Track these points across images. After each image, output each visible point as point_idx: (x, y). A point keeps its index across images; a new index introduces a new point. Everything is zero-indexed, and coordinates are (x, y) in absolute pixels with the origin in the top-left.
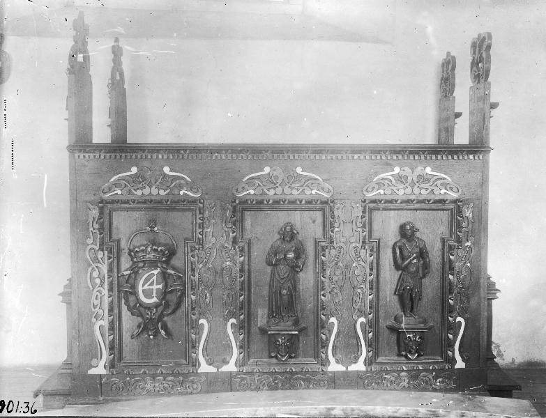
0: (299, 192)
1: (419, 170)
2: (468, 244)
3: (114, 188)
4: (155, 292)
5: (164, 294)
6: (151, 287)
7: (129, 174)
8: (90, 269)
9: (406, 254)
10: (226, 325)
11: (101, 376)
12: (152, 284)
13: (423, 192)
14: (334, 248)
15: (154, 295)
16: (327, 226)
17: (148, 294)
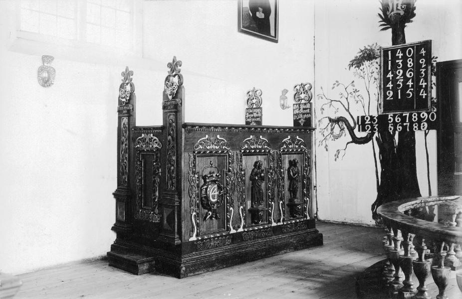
12: (215, 192)
15: (216, 197)
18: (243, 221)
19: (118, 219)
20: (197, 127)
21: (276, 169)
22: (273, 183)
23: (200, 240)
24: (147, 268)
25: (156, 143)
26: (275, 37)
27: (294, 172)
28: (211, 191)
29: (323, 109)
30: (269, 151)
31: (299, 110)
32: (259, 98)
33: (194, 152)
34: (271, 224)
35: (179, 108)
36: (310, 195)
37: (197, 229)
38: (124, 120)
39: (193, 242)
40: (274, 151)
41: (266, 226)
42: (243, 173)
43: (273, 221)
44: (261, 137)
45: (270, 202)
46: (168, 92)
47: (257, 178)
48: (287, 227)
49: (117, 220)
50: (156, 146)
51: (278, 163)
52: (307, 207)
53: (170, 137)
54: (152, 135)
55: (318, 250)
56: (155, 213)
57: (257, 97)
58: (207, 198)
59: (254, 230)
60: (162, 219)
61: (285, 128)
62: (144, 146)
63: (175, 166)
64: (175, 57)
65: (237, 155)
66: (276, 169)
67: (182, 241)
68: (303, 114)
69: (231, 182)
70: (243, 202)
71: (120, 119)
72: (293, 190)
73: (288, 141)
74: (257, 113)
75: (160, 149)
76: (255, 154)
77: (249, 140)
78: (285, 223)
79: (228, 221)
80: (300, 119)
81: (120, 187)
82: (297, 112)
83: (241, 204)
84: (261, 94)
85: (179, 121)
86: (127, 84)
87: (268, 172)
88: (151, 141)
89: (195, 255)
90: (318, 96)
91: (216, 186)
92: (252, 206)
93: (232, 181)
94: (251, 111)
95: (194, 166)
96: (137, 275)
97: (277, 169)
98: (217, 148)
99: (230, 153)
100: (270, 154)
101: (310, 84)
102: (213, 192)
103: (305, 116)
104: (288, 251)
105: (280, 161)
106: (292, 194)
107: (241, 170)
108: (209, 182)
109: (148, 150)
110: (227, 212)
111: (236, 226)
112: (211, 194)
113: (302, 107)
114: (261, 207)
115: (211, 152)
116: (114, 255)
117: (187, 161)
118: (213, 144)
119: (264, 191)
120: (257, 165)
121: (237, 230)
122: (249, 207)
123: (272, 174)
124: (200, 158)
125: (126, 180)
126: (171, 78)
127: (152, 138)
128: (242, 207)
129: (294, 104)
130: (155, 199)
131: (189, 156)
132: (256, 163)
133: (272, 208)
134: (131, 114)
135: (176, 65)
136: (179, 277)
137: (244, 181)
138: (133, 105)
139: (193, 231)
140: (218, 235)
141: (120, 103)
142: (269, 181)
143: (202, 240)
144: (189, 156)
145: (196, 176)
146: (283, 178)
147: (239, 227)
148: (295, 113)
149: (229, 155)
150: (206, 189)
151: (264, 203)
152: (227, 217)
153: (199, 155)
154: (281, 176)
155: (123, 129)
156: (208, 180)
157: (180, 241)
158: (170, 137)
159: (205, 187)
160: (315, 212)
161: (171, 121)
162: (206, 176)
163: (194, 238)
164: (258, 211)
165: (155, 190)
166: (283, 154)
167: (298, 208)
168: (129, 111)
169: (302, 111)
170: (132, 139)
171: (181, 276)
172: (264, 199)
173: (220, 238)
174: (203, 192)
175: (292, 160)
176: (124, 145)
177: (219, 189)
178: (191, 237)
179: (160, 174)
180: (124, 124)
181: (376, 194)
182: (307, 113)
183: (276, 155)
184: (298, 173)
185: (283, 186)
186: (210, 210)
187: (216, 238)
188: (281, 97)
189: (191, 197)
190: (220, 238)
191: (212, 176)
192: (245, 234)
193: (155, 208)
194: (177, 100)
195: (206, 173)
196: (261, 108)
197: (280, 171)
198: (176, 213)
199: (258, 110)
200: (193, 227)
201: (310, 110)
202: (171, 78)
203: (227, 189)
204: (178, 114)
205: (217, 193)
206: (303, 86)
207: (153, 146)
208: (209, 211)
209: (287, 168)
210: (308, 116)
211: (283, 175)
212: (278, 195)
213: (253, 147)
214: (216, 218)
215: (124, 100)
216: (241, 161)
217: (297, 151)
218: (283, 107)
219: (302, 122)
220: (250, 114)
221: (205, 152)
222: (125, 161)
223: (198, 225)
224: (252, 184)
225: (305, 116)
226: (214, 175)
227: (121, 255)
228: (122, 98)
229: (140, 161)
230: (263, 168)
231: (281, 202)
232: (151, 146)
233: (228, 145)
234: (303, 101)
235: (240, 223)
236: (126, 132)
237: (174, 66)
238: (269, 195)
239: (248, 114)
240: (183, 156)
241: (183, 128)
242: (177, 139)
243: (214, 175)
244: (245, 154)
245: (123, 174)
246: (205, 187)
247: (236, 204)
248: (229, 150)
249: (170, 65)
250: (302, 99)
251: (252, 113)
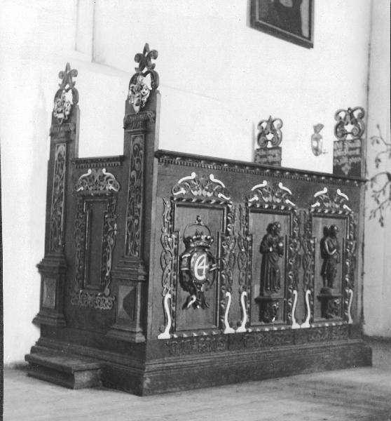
6: (202, 267)
12: (203, 265)
18: (246, 316)
19: (43, 306)
20: (178, 158)
21: (302, 239)
22: (296, 259)
23: (176, 339)
24: (89, 379)
25: (111, 182)
26: (310, 38)
27: (332, 246)
28: (197, 262)
29: (379, 160)
30: (293, 209)
31: (343, 150)
32: (278, 132)
33: (172, 198)
34: (292, 324)
35: (150, 126)
36: (354, 285)
37: (172, 322)
38: (60, 148)
39: (163, 341)
40: (300, 209)
41: (283, 328)
42: (249, 239)
43: (294, 320)
44: (281, 185)
45: (291, 291)
46: (135, 101)
47: (271, 250)
48: (317, 333)
49: (42, 307)
50: (111, 187)
51: (305, 230)
52: (350, 303)
53: (134, 173)
54: (104, 170)
55: (363, 370)
56: (104, 295)
57: (274, 132)
58: (190, 273)
59: (263, 332)
60: (115, 305)
61: (319, 175)
62: (91, 189)
63: (140, 218)
64: (147, 45)
65: (240, 209)
66: (302, 239)
67: (146, 338)
68: (349, 157)
69: (229, 252)
70: (248, 285)
71: (53, 146)
72: (328, 274)
73: (324, 196)
74: (274, 156)
75: (117, 194)
76: (269, 211)
77: (261, 189)
78: (313, 326)
79: (222, 313)
80: (343, 165)
81: (49, 254)
82: (339, 153)
83: (245, 289)
84: (282, 126)
85: (150, 147)
86: (67, 91)
87: (290, 242)
88: (102, 181)
89: (170, 361)
90: (372, 138)
91: (205, 255)
92: (261, 294)
93: (231, 251)
94: (263, 153)
95: (172, 220)
96: (72, 388)
97: (304, 238)
98: (209, 195)
99: (230, 206)
100: (295, 214)
101: (362, 109)
102: (200, 265)
103: (352, 160)
104: (317, 370)
105: (309, 225)
107: (247, 234)
108: (194, 248)
109: (96, 195)
110: (221, 299)
111: (235, 322)
112: (196, 268)
113: (347, 145)
114: (274, 296)
115: (199, 201)
116: (34, 359)
117: (160, 211)
118: (203, 188)
119: (282, 272)
120: (272, 229)
121: (235, 329)
122: (256, 294)
123: (295, 246)
124: (181, 209)
125: (60, 244)
126: (140, 78)
127: (104, 176)
128: (245, 293)
129: (335, 142)
130: (105, 272)
131: (164, 203)
132: (270, 226)
133: (293, 300)
134: (72, 138)
135: (149, 57)
136: (139, 393)
137: (251, 251)
138: (75, 125)
139: (165, 323)
140: (205, 334)
141: (55, 120)
142: (291, 256)
143: (181, 338)
144: (164, 203)
145: (174, 236)
146: (314, 253)
147: (239, 325)
148: (336, 155)
149: (228, 208)
150: (190, 258)
151: (281, 291)
152: (221, 307)
153: (180, 203)
154: (310, 250)
155: (58, 163)
156: (192, 245)
157: (143, 339)
158: (134, 173)
159: (187, 255)
160: (362, 241)
161: (136, 146)
162: (190, 238)
163: (165, 335)
164: (271, 301)
165: (105, 257)
166: (315, 216)
167: (335, 303)
168: (68, 133)
169: (346, 152)
170: (70, 180)
171: (145, 393)
172: (282, 283)
173: (208, 339)
174: (184, 263)
175: (329, 227)
176: (58, 188)
177: (209, 261)
178: (161, 331)
179: (115, 232)
180: (59, 155)
182: (356, 156)
183: (302, 217)
184: (338, 248)
185: (314, 266)
186: (194, 292)
187: (202, 339)
188: (313, 136)
189: (163, 270)
190: (208, 339)
191: (199, 239)
192: (248, 337)
193: (104, 287)
194: (148, 113)
195: (190, 233)
196: (280, 149)
197: (309, 242)
198: (139, 296)
199: (275, 152)
200: (166, 318)
201: (361, 151)
202: (140, 78)
203: (222, 262)
204: (149, 135)
205: (206, 267)
206: (350, 112)
207: (105, 189)
208: (192, 294)
209: (320, 240)
210: (355, 160)
211: (313, 249)
212: (304, 280)
213: (266, 200)
214: (203, 306)
215: (61, 116)
216: (247, 221)
217: (337, 212)
218: (317, 151)
219: (346, 170)
220: (261, 157)
221: (189, 200)
222: (59, 213)
223: (174, 315)
224: (264, 258)
225: (352, 160)
226: (203, 237)
228: (58, 112)
229: (83, 213)
230: (281, 234)
231: (308, 292)
232: (102, 188)
233: (226, 192)
234: (349, 137)
235: (242, 319)
236: (62, 168)
237: (145, 59)
238: (289, 279)
239: (258, 157)
240: (153, 202)
241: (156, 157)
242: (145, 175)
243: (203, 237)
244: (254, 209)
245: (55, 235)
246: (187, 255)
247: (235, 286)
248: (229, 201)
249: (139, 58)
250: (347, 133)
251: (265, 156)
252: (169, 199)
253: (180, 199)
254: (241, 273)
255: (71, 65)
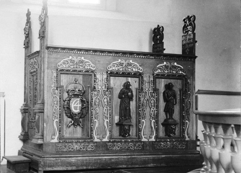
0: (82, 68)
1: (172, 64)
2: (189, 93)
3: (158, 69)
4: (78, 107)
5: (82, 109)
6: (77, 105)
7: (163, 64)
8: (103, 98)
9: (169, 95)
10: (53, 122)
11: (153, 142)
12: (77, 104)
13: (174, 72)
14: (144, 92)
15: (78, 108)
16: (141, 82)
17: (76, 108)
33: (57, 70)
37: (156, 133)
67: (43, 141)
82: (184, 42)
91: (79, 99)
106: (168, 115)
120: (127, 86)
129: (183, 36)
131: (52, 72)
144: (52, 72)
163: (56, 140)
167: (172, 127)
181: (26, 18)
189: (150, 108)
227: (167, 156)
247: (101, 117)
252: (56, 70)
253: (157, 75)
254: (104, 109)
255: (30, 10)
